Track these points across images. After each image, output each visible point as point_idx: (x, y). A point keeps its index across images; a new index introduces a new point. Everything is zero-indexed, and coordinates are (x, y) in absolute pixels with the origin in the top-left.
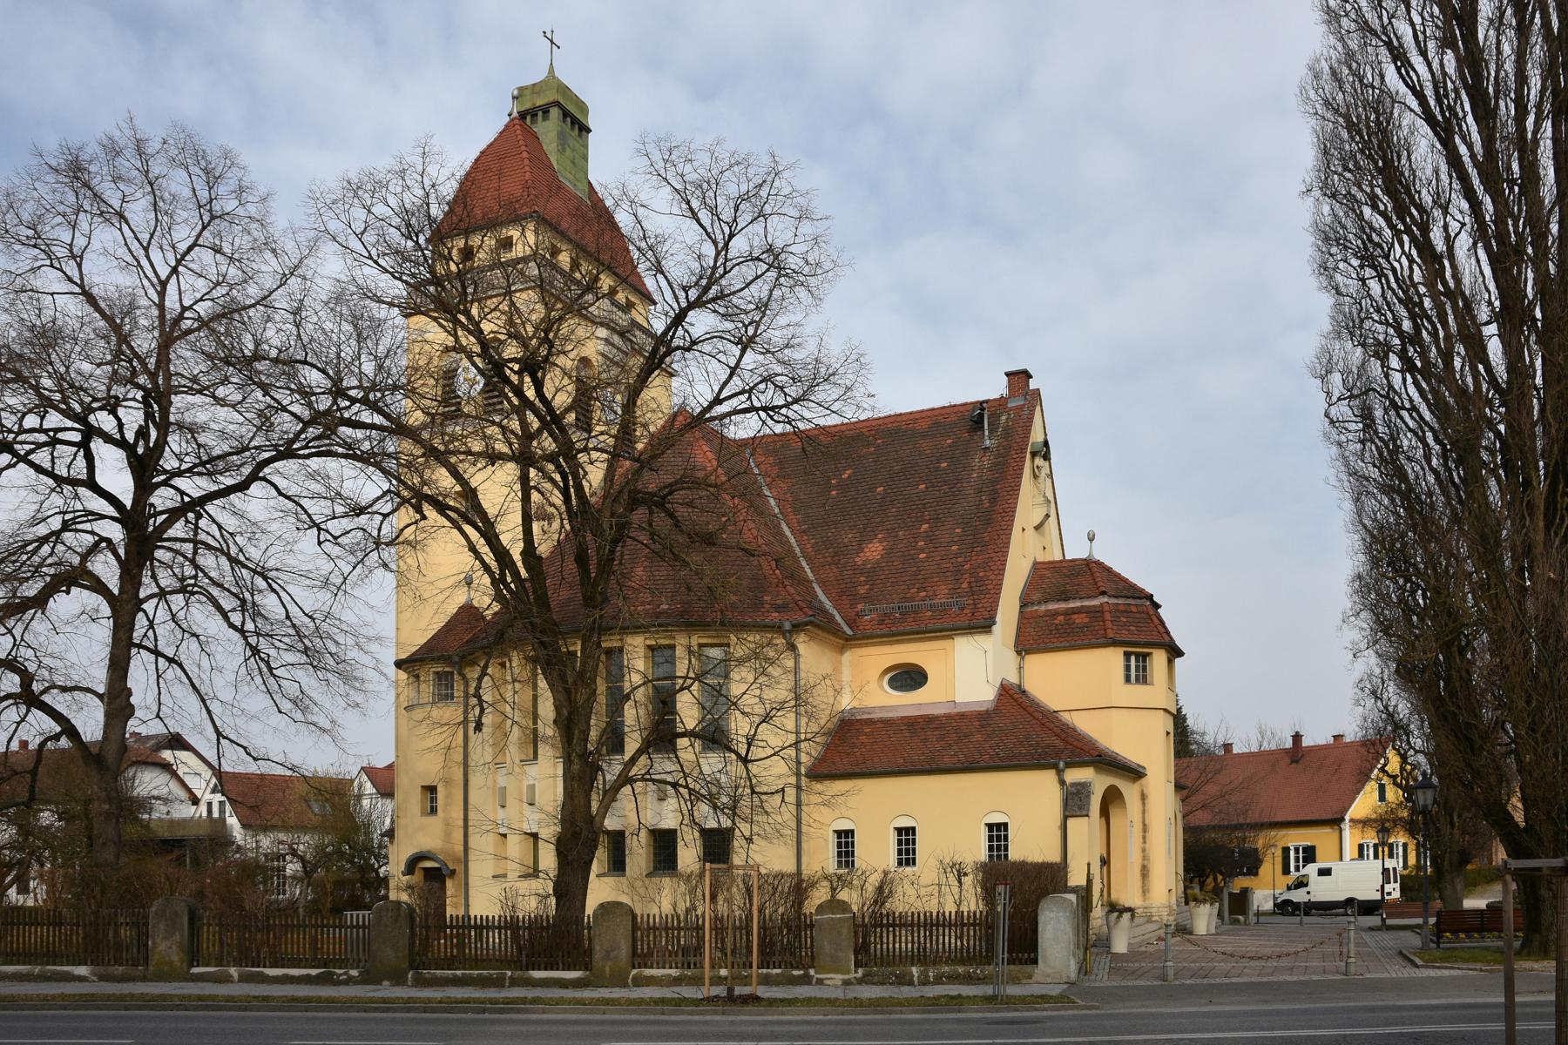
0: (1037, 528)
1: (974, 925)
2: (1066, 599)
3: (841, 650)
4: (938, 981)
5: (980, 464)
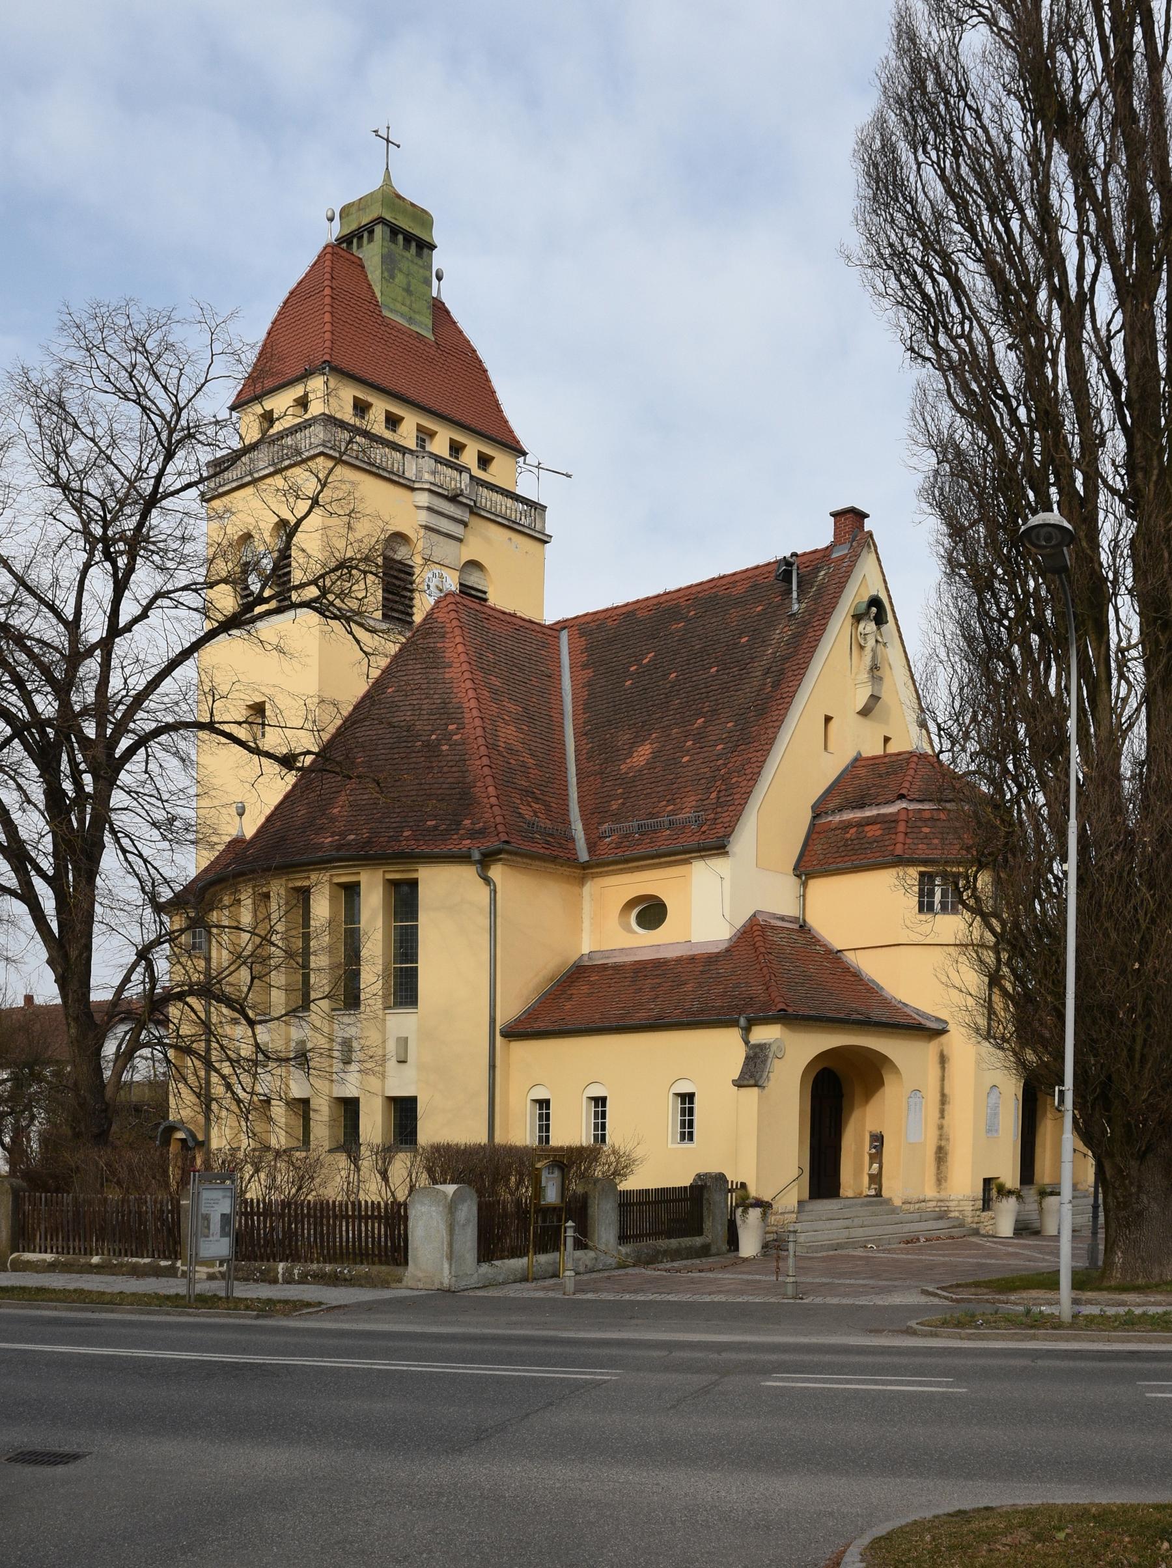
0: (865, 712)
1: (379, 1218)
2: (862, 806)
3: (582, 881)
4: (303, 1280)
5: (781, 633)
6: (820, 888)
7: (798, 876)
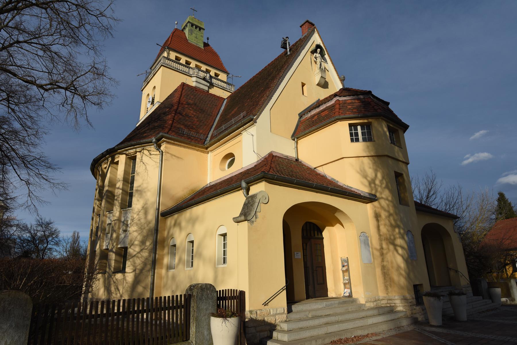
6: (305, 143)
7: (294, 140)
